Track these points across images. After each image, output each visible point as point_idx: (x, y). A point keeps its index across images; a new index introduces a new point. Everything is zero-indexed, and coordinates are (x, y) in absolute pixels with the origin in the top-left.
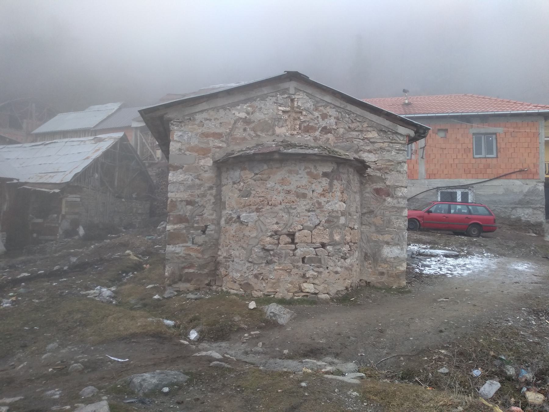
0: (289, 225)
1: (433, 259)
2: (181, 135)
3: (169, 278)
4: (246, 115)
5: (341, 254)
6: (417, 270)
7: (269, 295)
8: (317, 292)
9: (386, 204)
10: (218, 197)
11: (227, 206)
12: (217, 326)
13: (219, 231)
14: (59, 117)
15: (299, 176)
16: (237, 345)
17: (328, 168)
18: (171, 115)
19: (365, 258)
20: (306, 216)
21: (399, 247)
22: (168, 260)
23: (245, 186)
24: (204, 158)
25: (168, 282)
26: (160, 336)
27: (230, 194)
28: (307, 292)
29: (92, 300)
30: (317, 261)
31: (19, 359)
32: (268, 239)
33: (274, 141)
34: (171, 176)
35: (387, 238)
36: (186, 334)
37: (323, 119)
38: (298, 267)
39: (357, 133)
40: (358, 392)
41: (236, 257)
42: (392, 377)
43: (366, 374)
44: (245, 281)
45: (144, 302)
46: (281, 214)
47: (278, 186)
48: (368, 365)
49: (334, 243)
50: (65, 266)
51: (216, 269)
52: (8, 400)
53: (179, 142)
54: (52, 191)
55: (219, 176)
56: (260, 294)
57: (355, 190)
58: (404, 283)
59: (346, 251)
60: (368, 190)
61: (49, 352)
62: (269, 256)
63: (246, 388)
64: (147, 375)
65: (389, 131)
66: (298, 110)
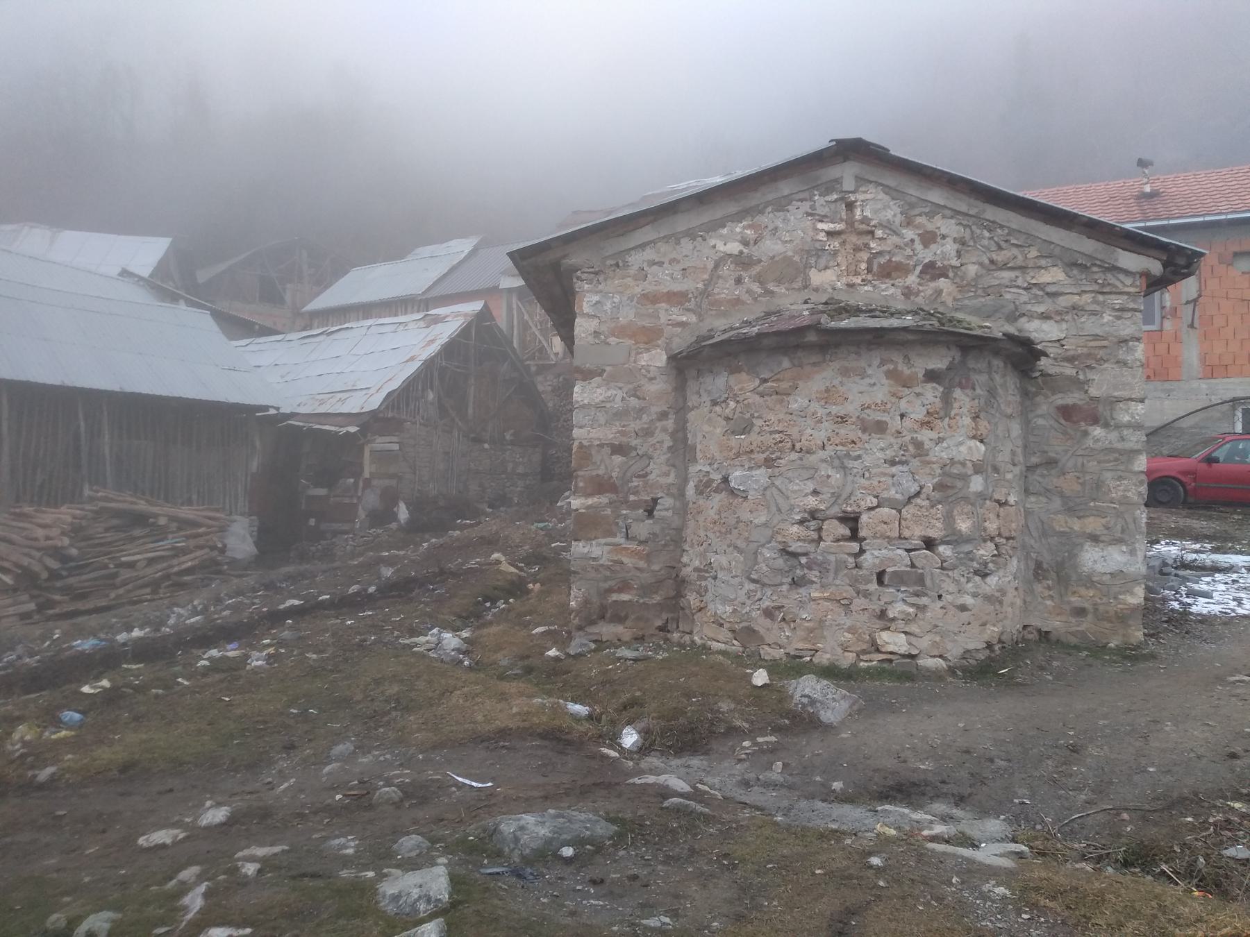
0: (844, 496)
1: (1218, 576)
2: (598, 302)
3: (578, 612)
4: (741, 247)
5: (975, 565)
6: (1175, 605)
7: (801, 657)
8: (914, 652)
9: (1089, 442)
10: (680, 435)
11: (699, 455)
12: (681, 720)
13: (683, 510)
14: (355, 274)
15: (867, 381)
16: (726, 764)
17: (939, 361)
18: (575, 258)
19: (1036, 575)
20: (885, 474)
21: (1124, 548)
22: (575, 572)
23: (739, 409)
24: (648, 350)
25: (576, 621)
26: (558, 738)
27: (706, 428)
28: (891, 653)
29: (422, 656)
30: (913, 580)
31: (280, 771)
32: (795, 528)
33: (806, 302)
34: (581, 393)
35: (1093, 524)
36: (614, 734)
37: (926, 246)
38: (867, 594)
39: (1012, 274)
40: (1008, 887)
41: (722, 569)
42: (1099, 859)
43: (1031, 848)
44: (744, 624)
45: (526, 662)
46: (825, 470)
47: (815, 406)
48: (1039, 827)
49: (955, 539)
50: (370, 585)
51: (679, 595)
52: (261, 852)
53: (595, 316)
54: (344, 430)
56: (778, 653)
57: (1009, 411)
58: (1138, 635)
59: (989, 559)
60: (1043, 409)
61: (336, 760)
62: (796, 567)
63: (743, 860)
64: (529, 819)
65: (1095, 265)
66: (864, 227)
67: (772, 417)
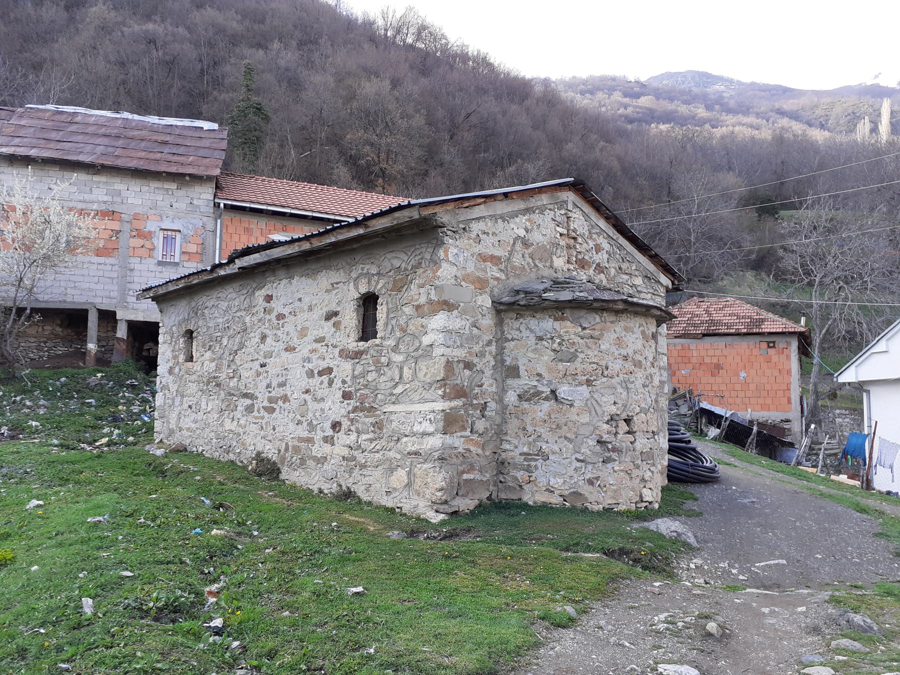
10: (499, 357)
32: (606, 426)
38: (638, 467)
44: (572, 490)
47: (613, 349)
55: (500, 323)
66: (574, 234)
67: (589, 352)
